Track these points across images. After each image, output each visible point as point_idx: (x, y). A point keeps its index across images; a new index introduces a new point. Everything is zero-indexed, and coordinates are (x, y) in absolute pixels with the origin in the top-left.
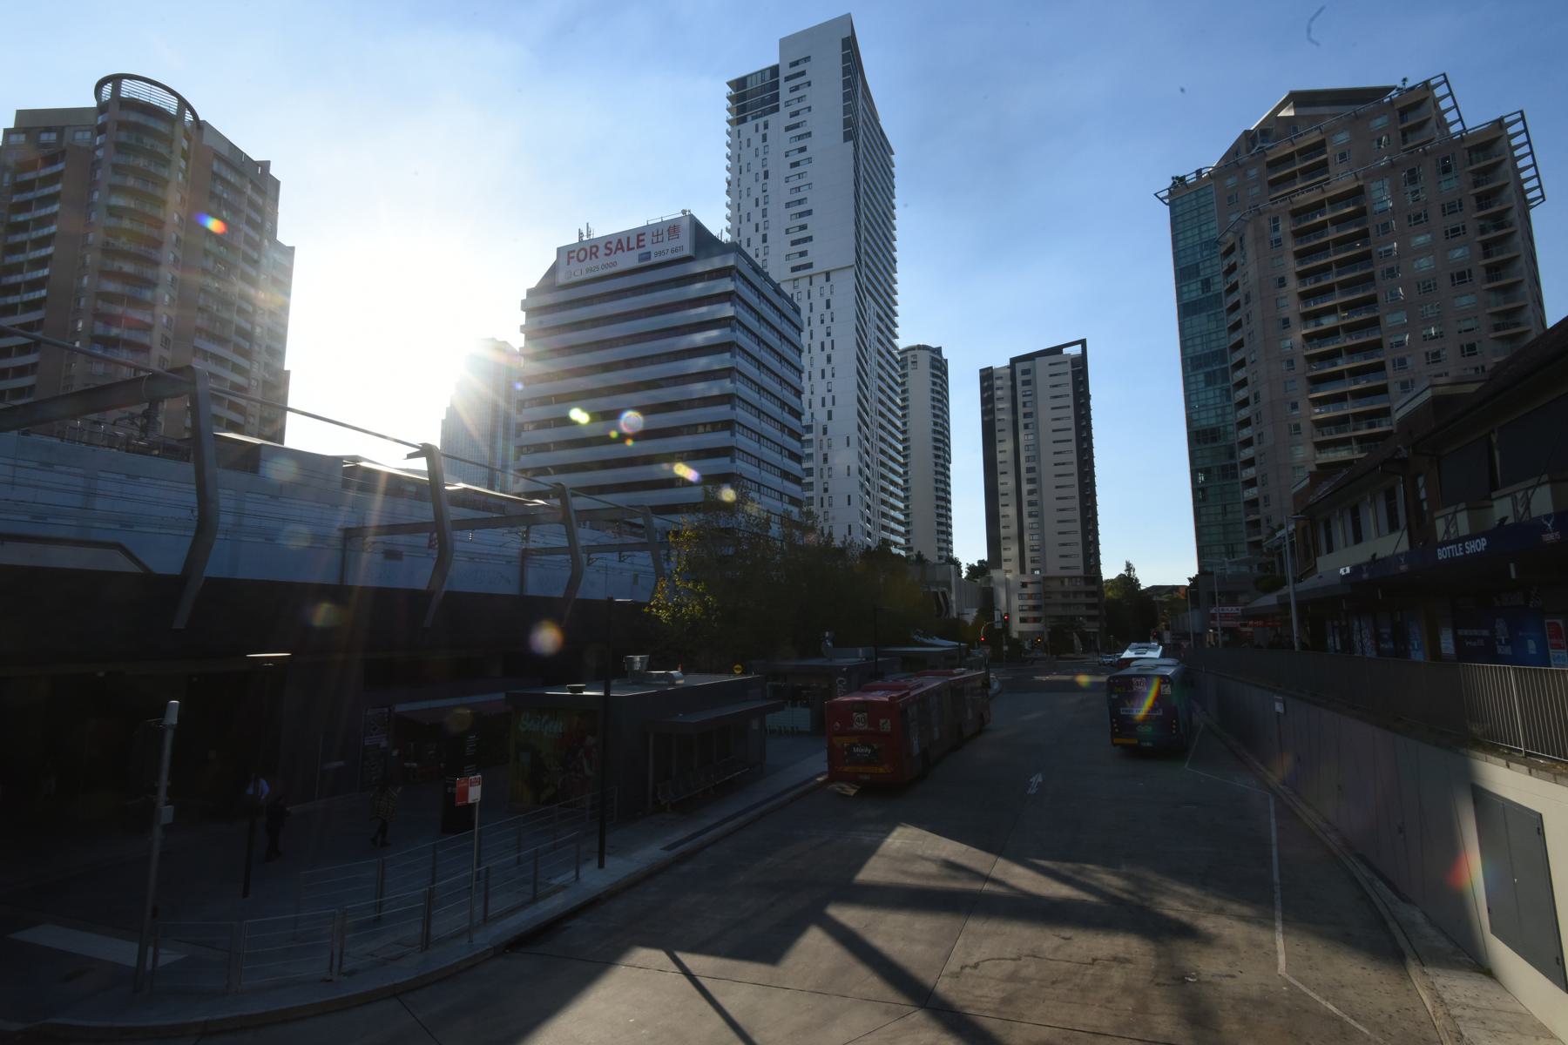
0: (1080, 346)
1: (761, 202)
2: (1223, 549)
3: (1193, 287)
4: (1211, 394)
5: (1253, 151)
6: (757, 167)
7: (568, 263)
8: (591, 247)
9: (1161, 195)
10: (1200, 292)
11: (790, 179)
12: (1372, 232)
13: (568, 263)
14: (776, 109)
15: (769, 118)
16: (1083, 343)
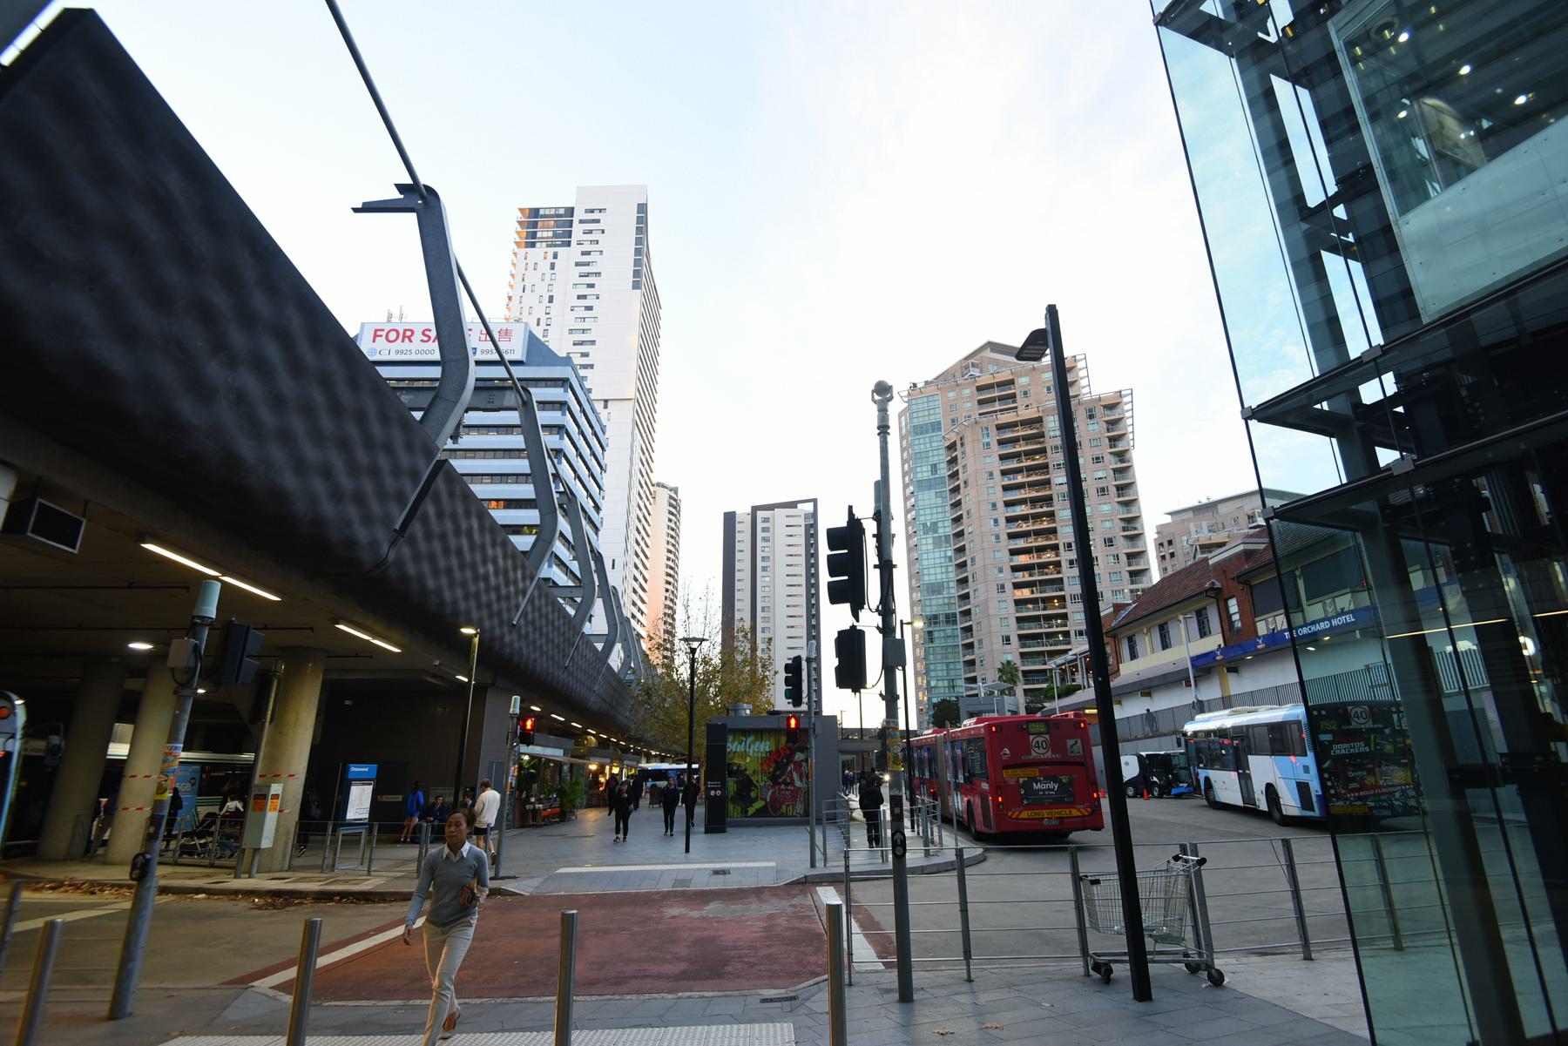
0: (812, 504)
1: (543, 323)
2: (946, 683)
3: (925, 469)
4: (937, 555)
5: (966, 377)
6: (542, 289)
7: (374, 341)
8: (405, 331)
9: (902, 394)
10: (930, 473)
11: (576, 309)
12: (1049, 450)
13: (374, 341)
14: (568, 244)
15: (561, 251)
16: (815, 501)
